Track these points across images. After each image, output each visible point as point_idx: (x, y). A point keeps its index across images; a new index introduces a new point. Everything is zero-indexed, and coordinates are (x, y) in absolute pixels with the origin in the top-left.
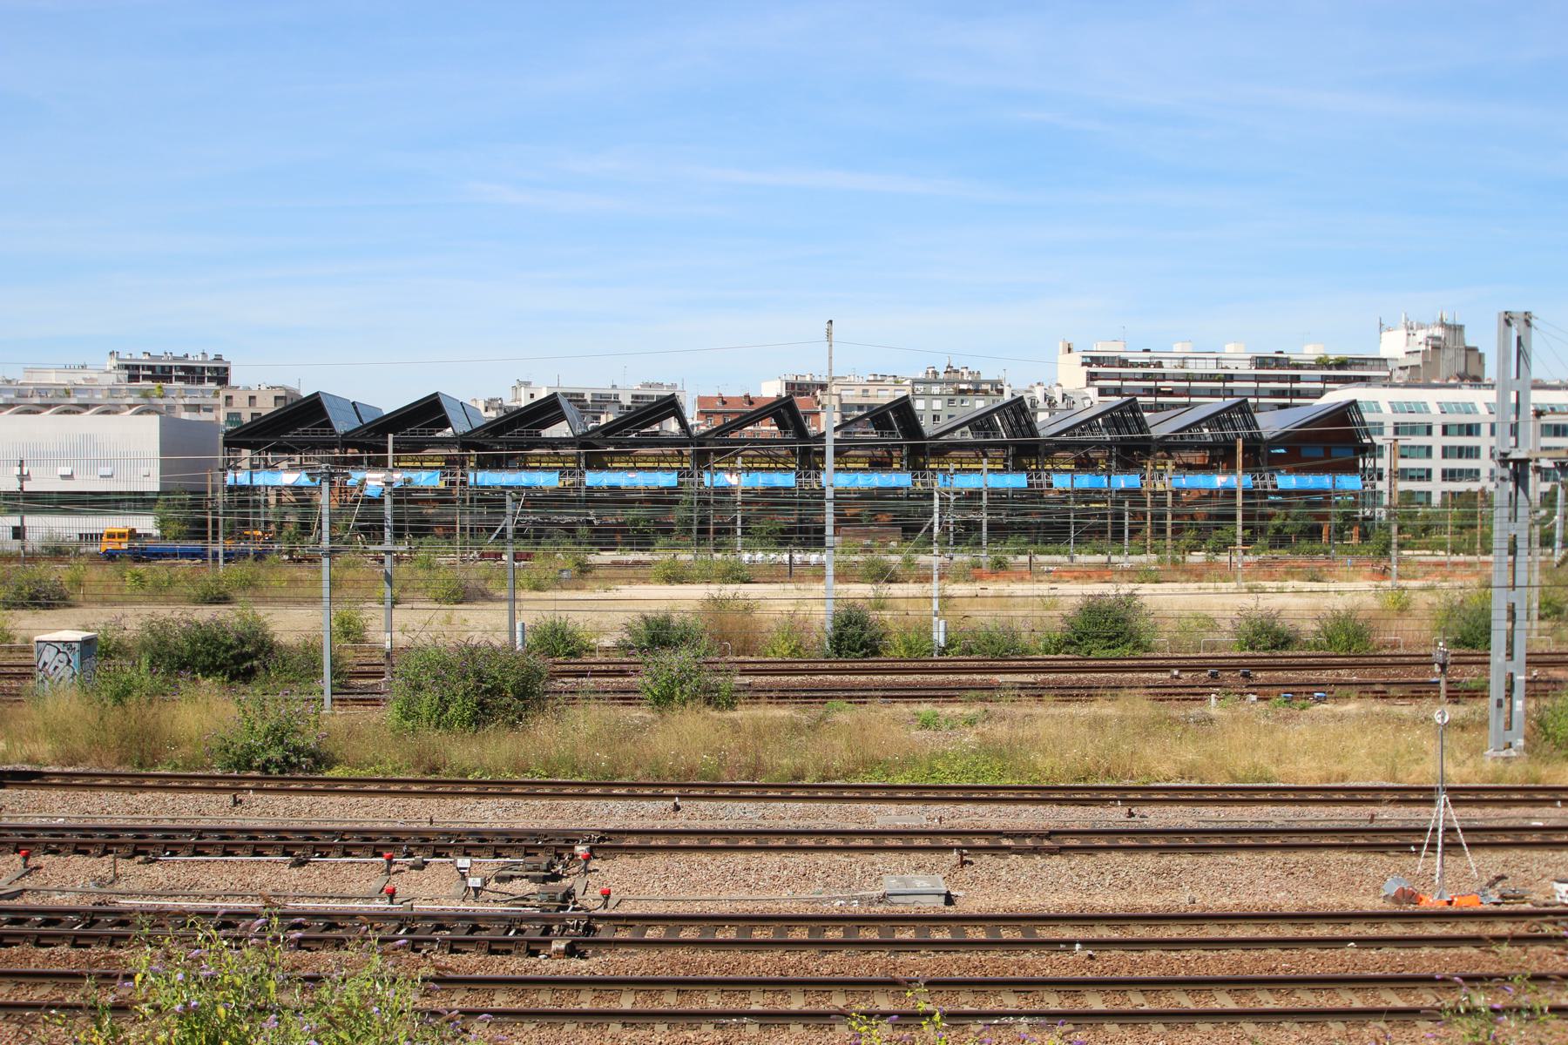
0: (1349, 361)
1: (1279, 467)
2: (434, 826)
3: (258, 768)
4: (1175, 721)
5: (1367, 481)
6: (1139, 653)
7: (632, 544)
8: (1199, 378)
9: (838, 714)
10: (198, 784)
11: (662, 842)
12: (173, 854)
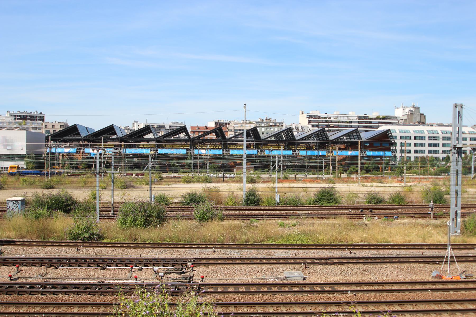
0: (386, 117)
1: (367, 149)
2: (141, 257)
3: (81, 239)
4: (355, 225)
5: (393, 153)
6: (337, 205)
7: (173, 171)
8: (342, 122)
9: (254, 223)
10: (64, 245)
12: (63, 266)
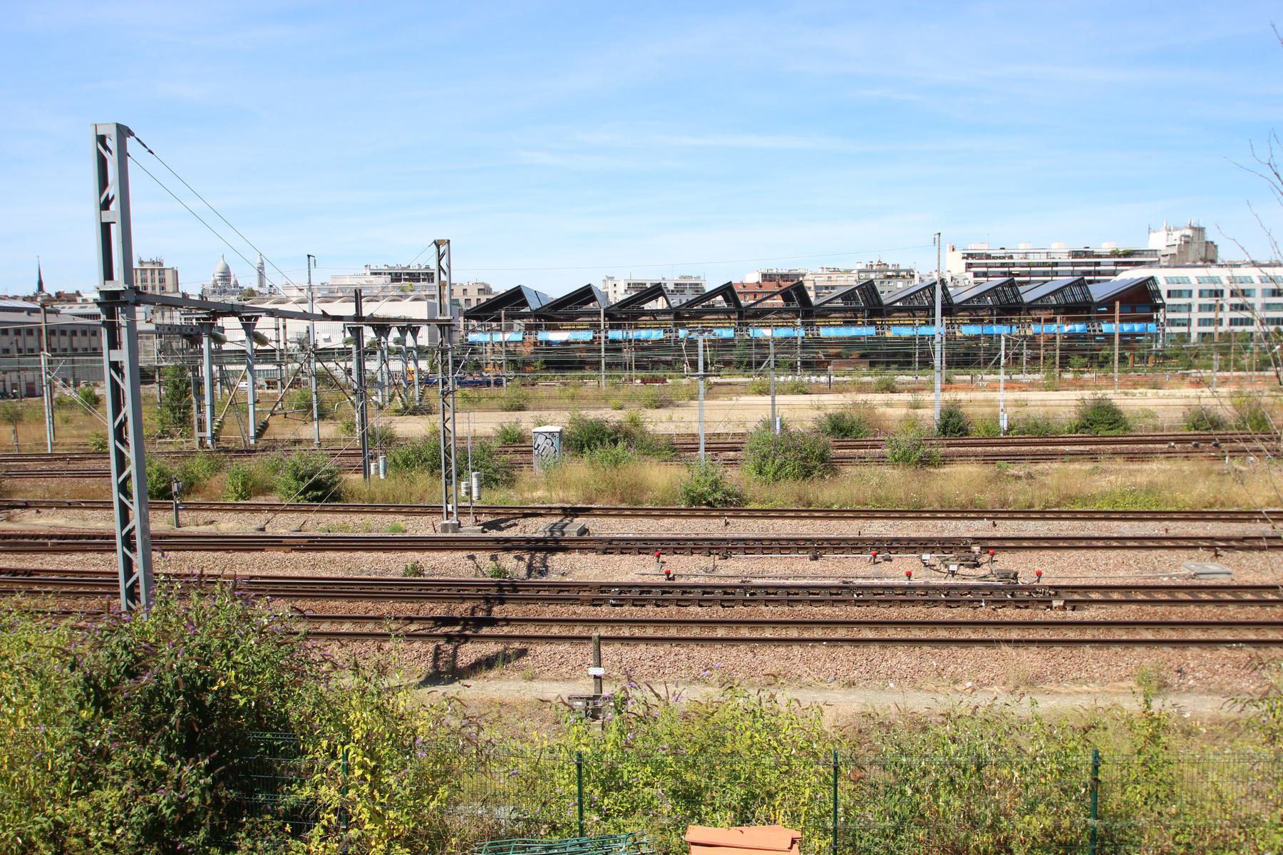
6: (1128, 433)
11: (1100, 544)
